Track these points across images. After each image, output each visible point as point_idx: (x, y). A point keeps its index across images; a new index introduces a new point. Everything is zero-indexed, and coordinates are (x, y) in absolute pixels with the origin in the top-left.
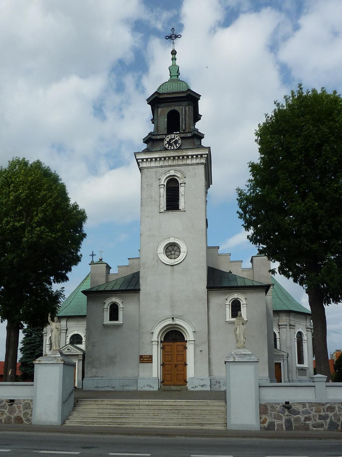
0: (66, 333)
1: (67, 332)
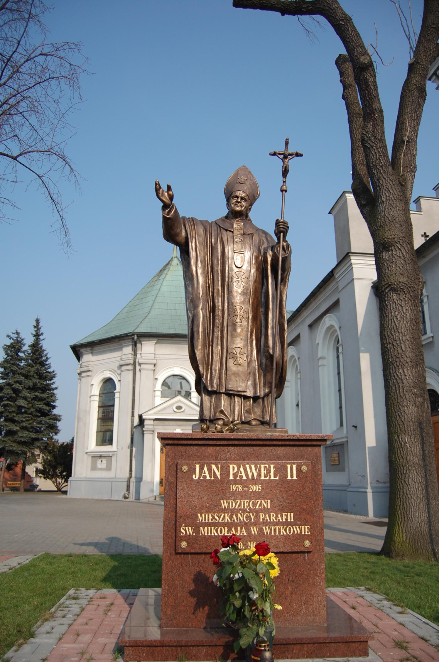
0: (154, 370)
1: (157, 369)
